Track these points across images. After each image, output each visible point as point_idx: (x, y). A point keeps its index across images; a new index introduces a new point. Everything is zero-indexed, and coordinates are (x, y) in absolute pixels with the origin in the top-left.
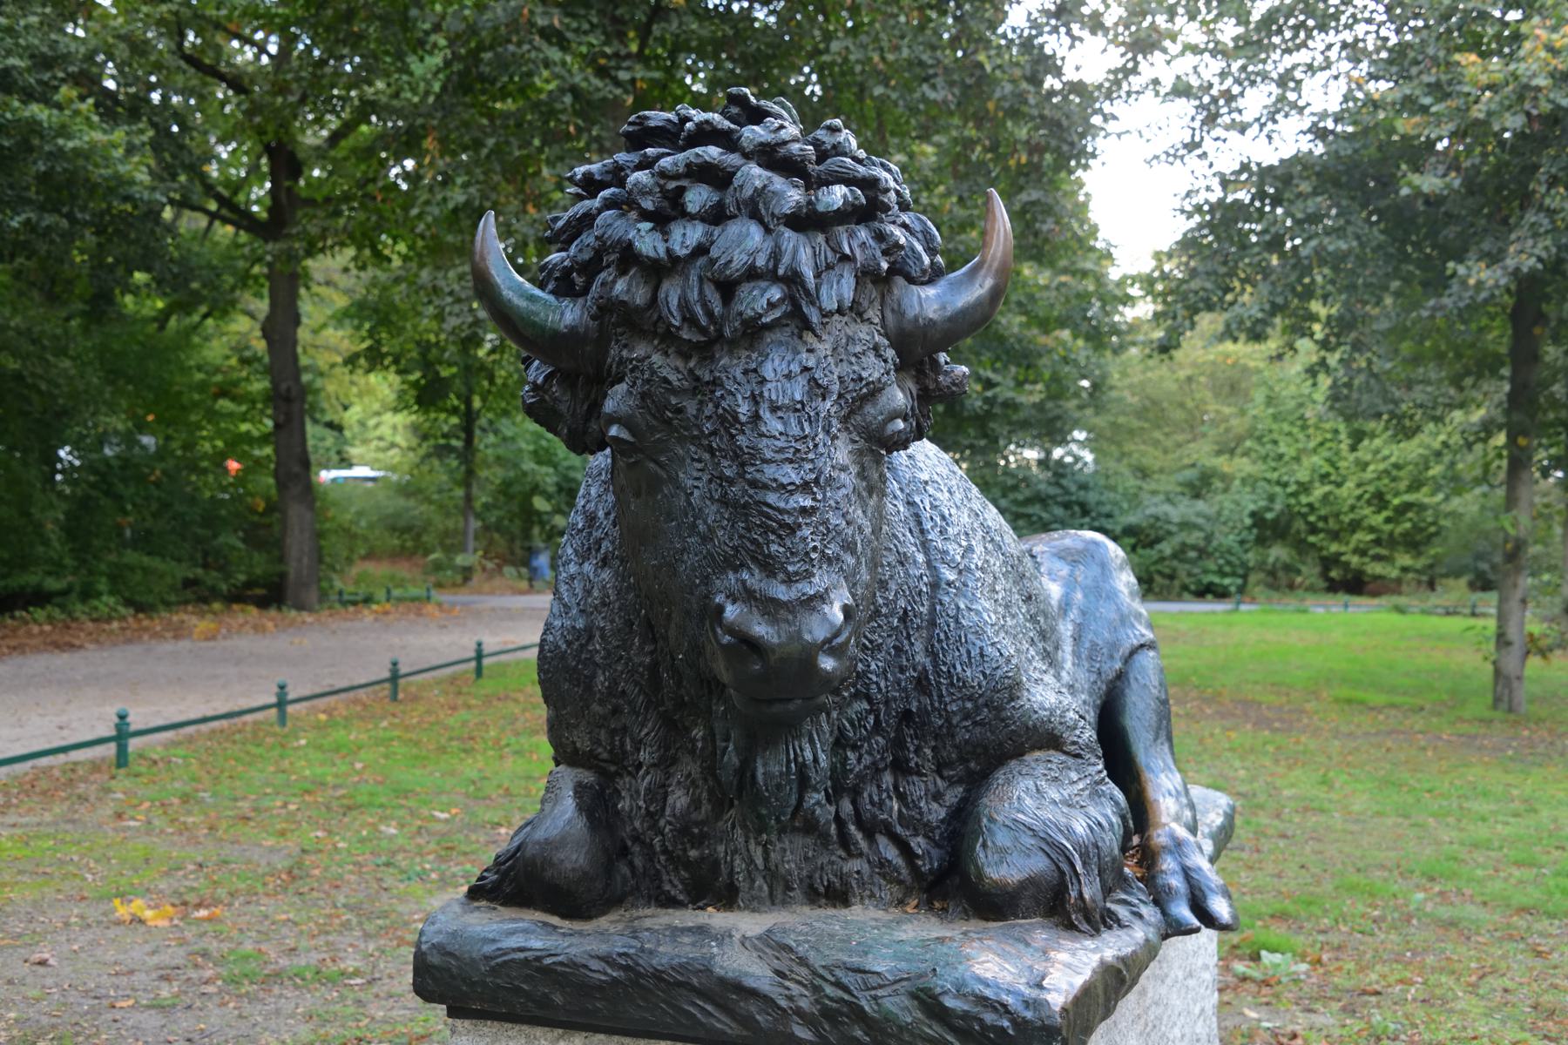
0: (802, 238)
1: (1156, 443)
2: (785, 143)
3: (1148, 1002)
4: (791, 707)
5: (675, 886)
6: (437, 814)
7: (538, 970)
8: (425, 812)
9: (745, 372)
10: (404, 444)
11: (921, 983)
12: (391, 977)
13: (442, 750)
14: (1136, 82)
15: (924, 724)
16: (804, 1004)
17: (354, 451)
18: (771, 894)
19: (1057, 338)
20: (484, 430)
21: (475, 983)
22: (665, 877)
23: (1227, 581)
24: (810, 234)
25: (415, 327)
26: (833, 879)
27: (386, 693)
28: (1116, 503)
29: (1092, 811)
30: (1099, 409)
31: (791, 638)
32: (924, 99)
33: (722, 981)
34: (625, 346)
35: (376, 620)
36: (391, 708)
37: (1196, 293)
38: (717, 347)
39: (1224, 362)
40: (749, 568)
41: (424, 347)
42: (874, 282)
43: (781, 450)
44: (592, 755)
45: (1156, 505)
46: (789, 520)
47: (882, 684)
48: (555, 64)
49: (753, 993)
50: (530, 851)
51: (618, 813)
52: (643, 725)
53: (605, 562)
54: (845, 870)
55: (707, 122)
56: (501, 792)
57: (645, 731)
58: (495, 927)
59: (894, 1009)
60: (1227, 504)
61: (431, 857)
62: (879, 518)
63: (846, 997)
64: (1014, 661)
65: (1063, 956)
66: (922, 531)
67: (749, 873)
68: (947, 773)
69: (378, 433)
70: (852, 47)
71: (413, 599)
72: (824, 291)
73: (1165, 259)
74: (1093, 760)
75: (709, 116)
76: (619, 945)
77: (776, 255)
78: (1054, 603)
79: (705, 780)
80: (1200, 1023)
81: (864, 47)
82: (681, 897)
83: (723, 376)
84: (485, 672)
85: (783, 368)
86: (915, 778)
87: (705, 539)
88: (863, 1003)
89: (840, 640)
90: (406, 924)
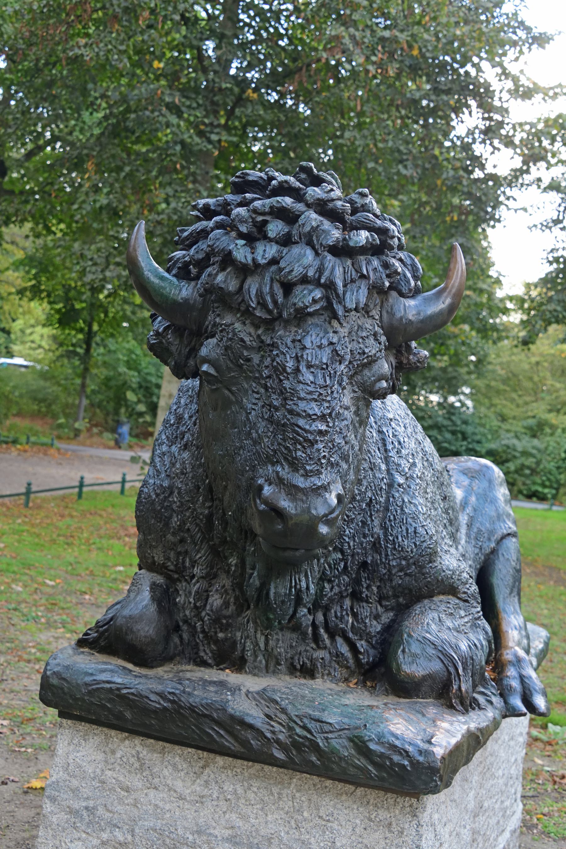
0: (338, 261)
1: (513, 400)
2: (333, 200)
3: (487, 753)
4: (298, 554)
5: (207, 654)
6: (48, 581)
7: (118, 696)
8: (40, 579)
9: (293, 341)
10: (47, 347)
11: (356, 733)
12: (13, 680)
13: (53, 541)
14: (527, 178)
15: (374, 571)
16: (281, 737)
17: (15, 348)
18: (267, 667)
19: (461, 329)
20: (97, 344)
21: (78, 699)
22: (201, 648)
23: (546, 491)
24: (343, 259)
25: (63, 276)
26: (306, 660)
27: (22, 501)
28: (484, 435)
29: (471, 636)
30: (480, 375)
31: (303, 511)
32: (398, 173)
33: (232, 717)
34: (219, 315)
35: (19, 455)
36: (24, 511)
37: (550, 312)
38: (277, 323)
39: (560, 355)
40: (282, 465)
41: (67, 289)
42: (378, 293)
43: (311, 393)
44: (164, 566)
45: (508, 439)
46: (311, 437)
47: (352, 544)
48: (173, 125)
49: (251, 727)
50: (120, 621)
51: (176, 604)
52: (198, 552)
53: (185, 447)
54: (314, 656)
55: (286, 182)
56: (88, 572)
57: (199, 555)
58: (93, 666)
59: (338, 747)
60: (552, 443)
61: (42, 608)
62: (363, 440)
63: (309, 736)
64: (435, 538)
65: (445, 725)
66: (386, 450)
67: (255, 651)
68: (385, 603)
69: (31, 338)
70: (358, 137)
71: (43, 444)
72: (348, 295)
73: (533, 288)
74: (475, 604)
75: (288, 178)
76: (169, 687)
77: (320, 270)
78: (458, 501)
79: (234, 590)
80: (514, 768)
81: (365, 137)
82: (210, 661)
83: (279, 342)
84: (84, 495)
85: (317, 341)
86: (365, 604)
87: (256, 443)
88: (319, 741)
89: (333, 516)
90: (24, 648)
